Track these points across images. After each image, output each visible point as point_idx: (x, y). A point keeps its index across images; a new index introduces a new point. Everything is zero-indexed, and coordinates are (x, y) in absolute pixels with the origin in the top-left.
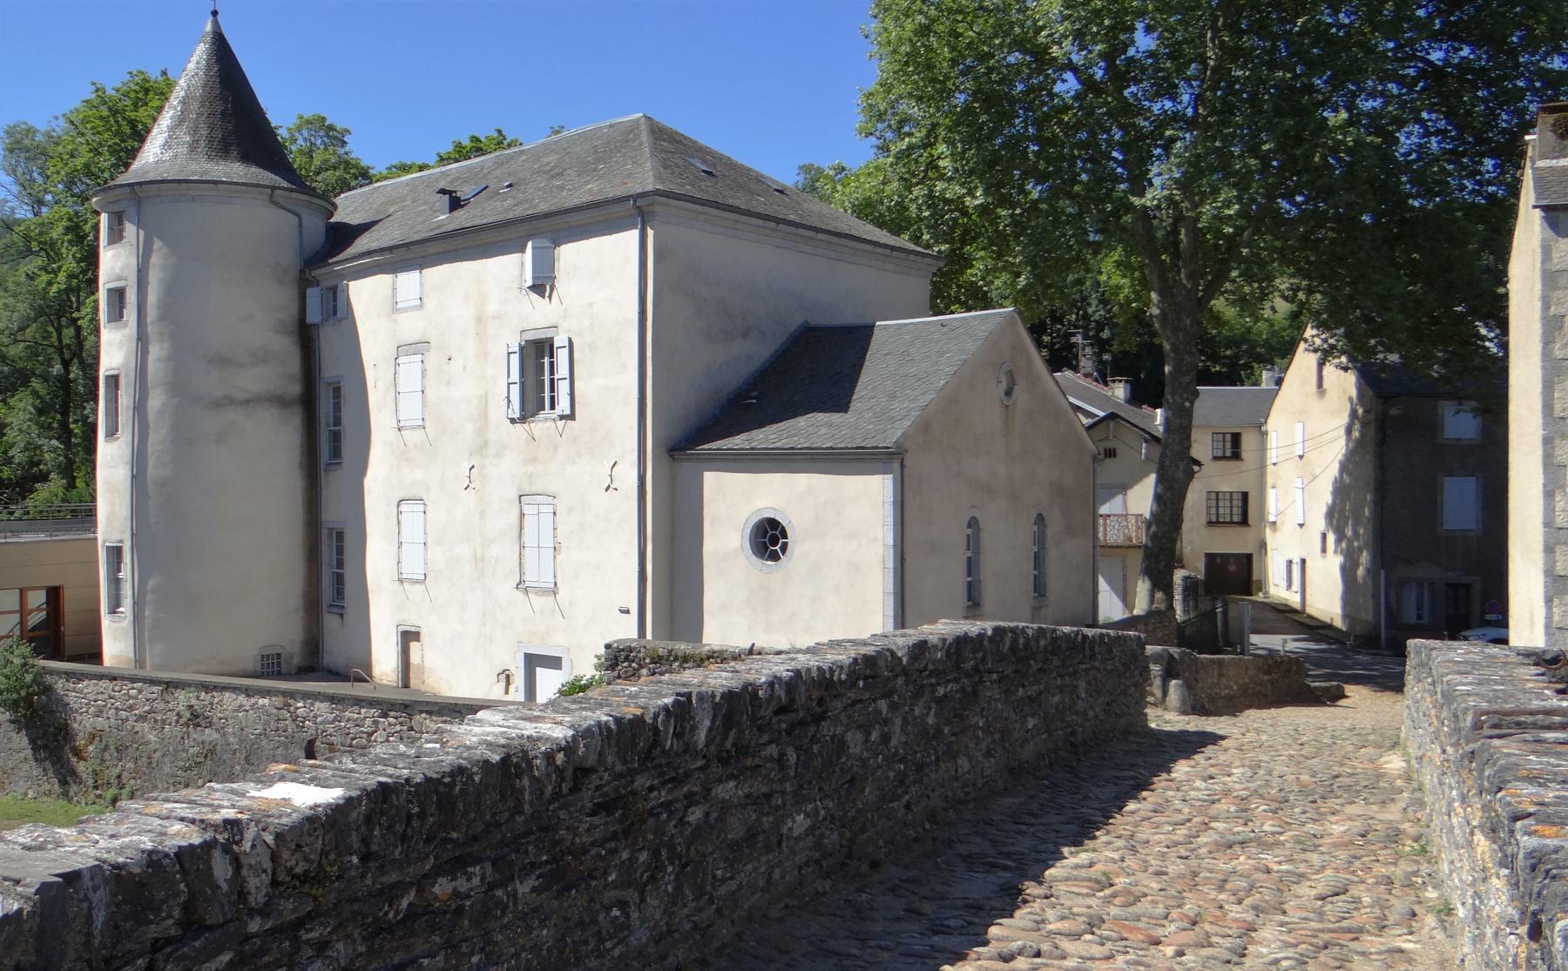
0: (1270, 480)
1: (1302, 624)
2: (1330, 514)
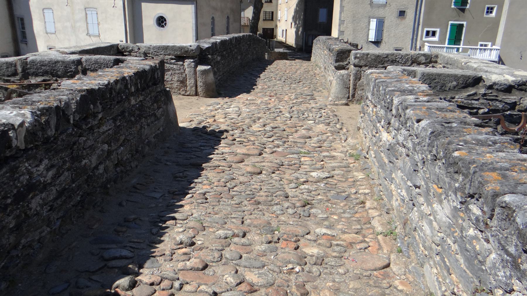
0: (279, 8)
1: (286, 46)
2: (293, 18)
